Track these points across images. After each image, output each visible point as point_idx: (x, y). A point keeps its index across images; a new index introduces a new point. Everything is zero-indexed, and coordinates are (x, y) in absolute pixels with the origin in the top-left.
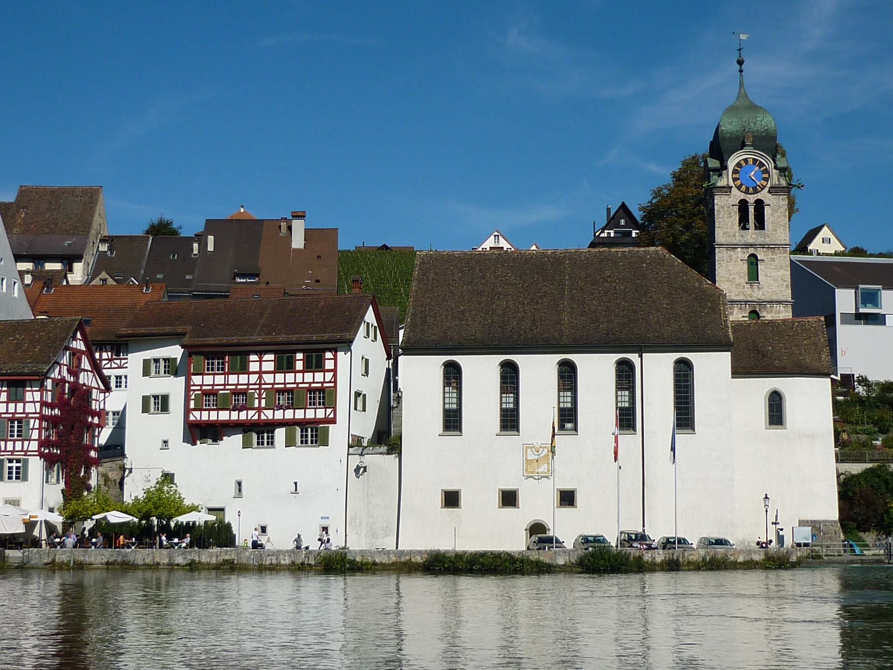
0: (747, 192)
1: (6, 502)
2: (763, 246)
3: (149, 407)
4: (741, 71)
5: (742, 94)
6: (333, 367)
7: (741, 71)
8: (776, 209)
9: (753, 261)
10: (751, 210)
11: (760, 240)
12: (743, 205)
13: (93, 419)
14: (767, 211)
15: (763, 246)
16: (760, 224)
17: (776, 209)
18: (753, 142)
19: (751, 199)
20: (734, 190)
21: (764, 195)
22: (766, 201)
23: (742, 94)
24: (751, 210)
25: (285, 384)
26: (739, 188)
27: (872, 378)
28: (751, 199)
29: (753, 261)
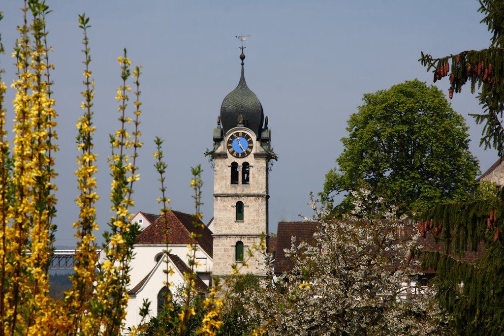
0: (237, 156)
1: (422, 52)
2: (248, 196)
3: (237, 180)
4: (243, 64)
5: (25, 12)
6: (262, 191)
7: (243, 64)
8: (257, 168)
9: (240, 207)
10: (240, 170)
11: (246, 191)
12: (234, 166)
13: (139, 177)
14: (251, 171)
15: (248, 196)
16: (246, 181)
17: (257, 168)
18: (244, 121)
19: (240, 162)
20: (229, 155)
21: (250, 159)
22: (251, 164)
23: (25, 12)
24: (240, 170)
25: (167, 246)
26: (232, 153)
27: (454, 54)
28: (240, 162)
29: (240, 207)
